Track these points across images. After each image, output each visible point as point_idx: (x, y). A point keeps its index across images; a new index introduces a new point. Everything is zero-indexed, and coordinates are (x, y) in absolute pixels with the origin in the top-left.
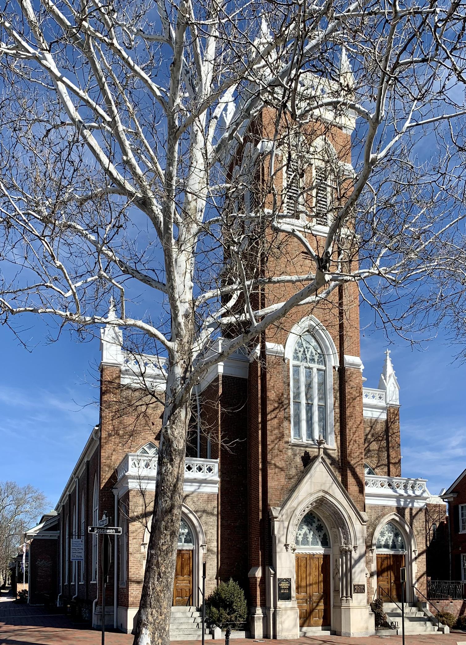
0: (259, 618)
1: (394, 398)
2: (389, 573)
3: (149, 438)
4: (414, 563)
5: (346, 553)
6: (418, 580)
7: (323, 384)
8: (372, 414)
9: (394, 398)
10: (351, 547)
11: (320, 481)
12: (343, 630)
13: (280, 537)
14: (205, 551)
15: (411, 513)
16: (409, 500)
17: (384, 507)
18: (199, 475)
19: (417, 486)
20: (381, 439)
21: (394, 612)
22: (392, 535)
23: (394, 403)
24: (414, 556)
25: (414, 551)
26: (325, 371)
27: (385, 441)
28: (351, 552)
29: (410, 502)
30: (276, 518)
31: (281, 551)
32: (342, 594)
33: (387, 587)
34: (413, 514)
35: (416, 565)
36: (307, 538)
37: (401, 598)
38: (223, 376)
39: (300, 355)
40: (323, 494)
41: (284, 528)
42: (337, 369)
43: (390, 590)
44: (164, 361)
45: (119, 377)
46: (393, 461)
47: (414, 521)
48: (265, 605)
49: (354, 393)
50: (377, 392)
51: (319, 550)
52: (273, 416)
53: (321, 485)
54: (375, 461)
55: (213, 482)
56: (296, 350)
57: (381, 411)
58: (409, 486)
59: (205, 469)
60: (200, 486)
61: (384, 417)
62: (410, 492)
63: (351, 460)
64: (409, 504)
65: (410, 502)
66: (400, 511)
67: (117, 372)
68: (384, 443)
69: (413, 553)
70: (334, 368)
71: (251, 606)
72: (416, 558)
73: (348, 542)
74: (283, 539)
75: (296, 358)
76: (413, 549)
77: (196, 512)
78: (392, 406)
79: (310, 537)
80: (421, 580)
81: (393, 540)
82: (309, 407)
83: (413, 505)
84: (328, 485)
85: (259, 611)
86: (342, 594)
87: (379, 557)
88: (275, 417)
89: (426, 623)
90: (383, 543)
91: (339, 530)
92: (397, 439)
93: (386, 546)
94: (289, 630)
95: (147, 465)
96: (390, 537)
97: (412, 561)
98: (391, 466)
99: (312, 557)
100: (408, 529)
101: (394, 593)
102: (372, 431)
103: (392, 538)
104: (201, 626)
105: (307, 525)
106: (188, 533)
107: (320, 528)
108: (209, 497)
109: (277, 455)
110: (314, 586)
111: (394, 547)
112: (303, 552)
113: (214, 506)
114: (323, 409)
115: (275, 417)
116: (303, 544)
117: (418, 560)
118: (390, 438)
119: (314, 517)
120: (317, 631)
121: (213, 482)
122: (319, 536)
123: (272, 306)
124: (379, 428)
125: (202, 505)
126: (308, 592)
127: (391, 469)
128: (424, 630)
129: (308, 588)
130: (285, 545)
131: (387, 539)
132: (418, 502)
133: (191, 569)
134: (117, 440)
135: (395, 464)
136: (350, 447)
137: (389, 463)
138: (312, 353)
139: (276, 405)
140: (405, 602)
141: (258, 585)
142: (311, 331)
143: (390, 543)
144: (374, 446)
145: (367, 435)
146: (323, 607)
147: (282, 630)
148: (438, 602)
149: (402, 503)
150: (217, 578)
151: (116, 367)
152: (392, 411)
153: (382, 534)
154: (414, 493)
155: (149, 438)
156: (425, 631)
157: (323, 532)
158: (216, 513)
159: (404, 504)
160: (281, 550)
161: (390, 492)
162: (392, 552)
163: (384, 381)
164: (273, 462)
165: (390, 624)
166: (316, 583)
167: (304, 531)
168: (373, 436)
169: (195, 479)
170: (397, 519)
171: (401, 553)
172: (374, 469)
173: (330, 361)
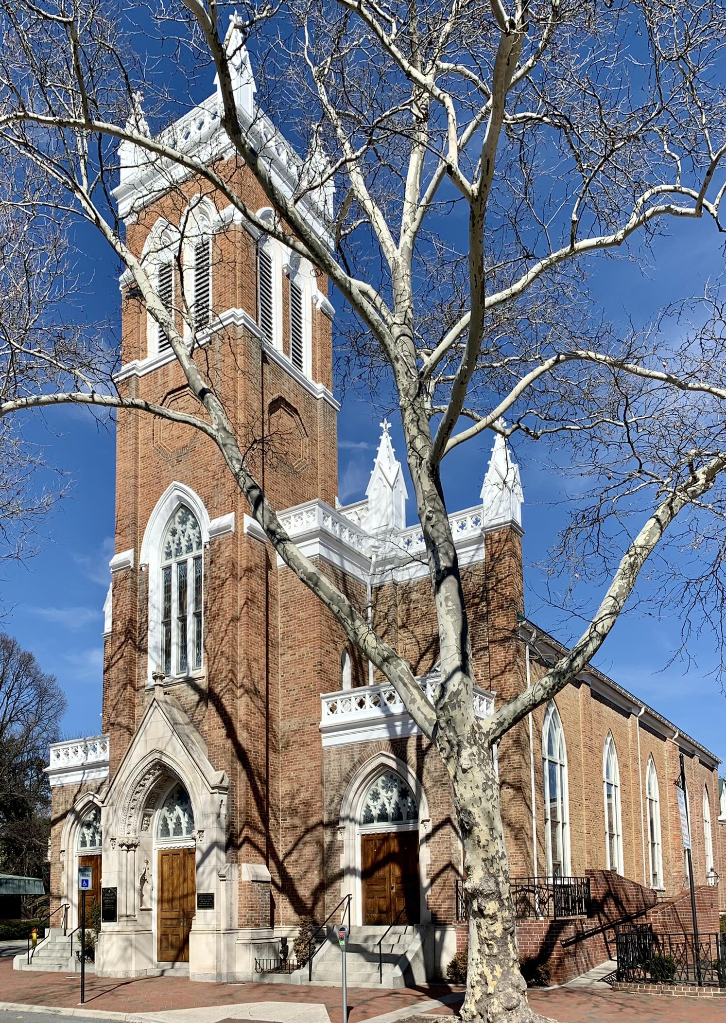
6: (433, 881)
17: (365, 744)
20: (477, 600)
22: (394, 794)
34: (424, 746)
35: (428, 850)
40: (157, 756)
47: (427, 760)
57: (475, 547)
64: (412, 728)
66: (398, 746)
72: (428, 837)
80: (439, 881)
81: (397, 804)
87: (367, 840)
90: (375, 812)
93: (383, 817)
94: (114, 965)
95: (361, 704)
111: (397, 817)
116: (175, 834)
117: (432, 840)
143: (390, 810)
149: (399, 730)
152: (496, 536)
170: (393, 764)
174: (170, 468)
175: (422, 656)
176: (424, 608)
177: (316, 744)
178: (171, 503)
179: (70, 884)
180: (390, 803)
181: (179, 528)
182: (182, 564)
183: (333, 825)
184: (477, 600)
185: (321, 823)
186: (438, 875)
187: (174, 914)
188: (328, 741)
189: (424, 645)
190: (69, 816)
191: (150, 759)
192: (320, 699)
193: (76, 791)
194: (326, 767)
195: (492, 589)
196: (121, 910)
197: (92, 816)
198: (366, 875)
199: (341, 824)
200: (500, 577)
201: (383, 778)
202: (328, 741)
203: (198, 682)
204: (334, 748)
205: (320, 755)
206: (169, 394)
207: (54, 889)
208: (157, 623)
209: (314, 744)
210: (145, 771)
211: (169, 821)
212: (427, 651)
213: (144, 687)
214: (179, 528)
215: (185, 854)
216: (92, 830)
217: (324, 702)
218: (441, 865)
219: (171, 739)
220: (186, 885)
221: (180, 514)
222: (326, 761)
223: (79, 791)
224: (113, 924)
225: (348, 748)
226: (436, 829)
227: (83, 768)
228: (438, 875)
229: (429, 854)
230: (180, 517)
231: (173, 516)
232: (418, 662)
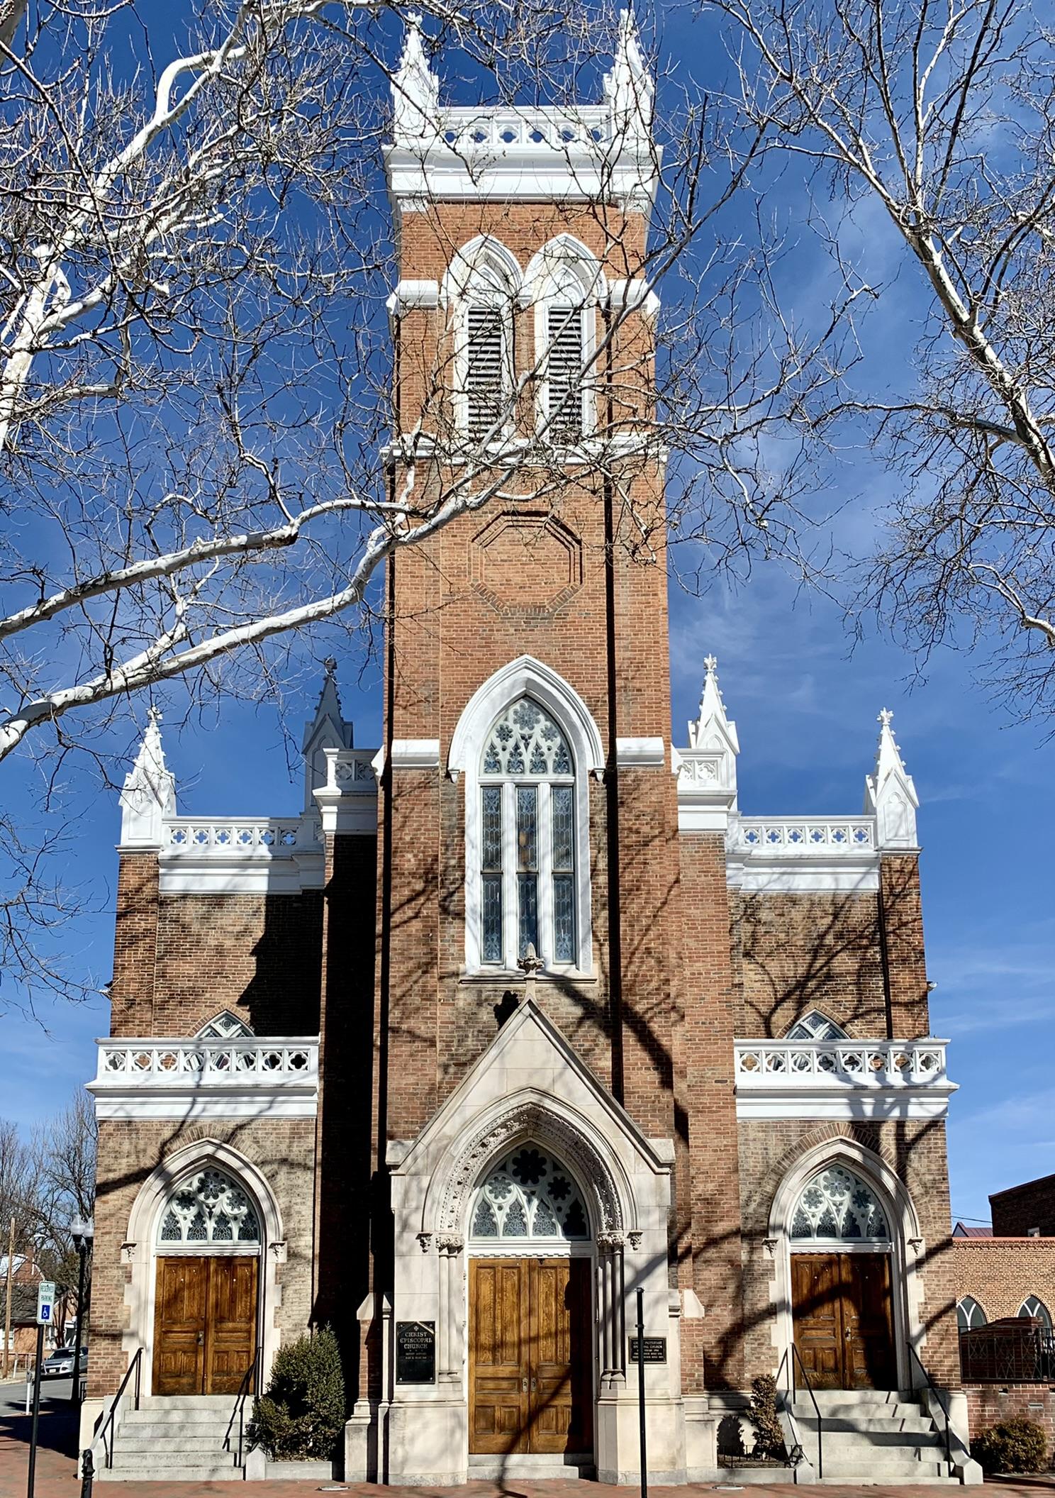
0: (357, 1428)
1: (902, 832)
2: (837, 1305)
3: (223, 1002)
4: (912, 1279)
5: (612, 1251)
6: (928, 1326)
7: (565, 821)
8: (836, 880)
9: (902, 832)
10: (622, 1236)
11: (528, 1064)
12: (602, 1467)
13: (409, 1215)
14: (282, 1258)
15: (900, 1136)
16: (890, 1100)
17: (809, 1123)
18: (272, 1077)
19: (917, 1062)
20: (865, 942)
21: (841, 1416)
22: (846, 1199)
23: (904, 845)
24: (911, 1256)
25: (911, 1242)
26: (573, 786)
27: (877, 949)
28: (622, 1248)
29: (893, 1105)
30: (396, 1167)
31: (410, 1252)
32: (605, 1367)
33: (831, 1345)
36: (523, 1215)
37: (882, 1378)
38: (338, 838)
39: (504, 757)
40: (534, 1098)
41: (420, 1191)
42: (600, 776)
43: (842, 1356)
44: (266, 825)
45: (157, 876)
46: (903, 998)
48: (375, 1396)
49: (646, 829)
50: (850, 824)
51: (558, 1246)
52: (410, 913)
53: (530, 1076)
54: (849, 1000)
55: (309, 1091)
56: (493, 747)
57: (863, 870)
58: (893, 1062)
59: (286, 1060)
60: (272, 1102)
61: (872, 884)
62: (895, 1079)
63: (637, 1003)
64: (890, 1110)
65: (893, 1105)
66: (865, 1132)
67: (152, 865)
68: (874, 954)
69: (909, 1248)
70: (593, 774)
71: (351, 1396)
72: (919, 1263)
73: (614, 1221)
74: (415, 1221)
75: (493, 764)
76: (909, 1233)
77: (263, 1163)
78: (897, 852)
79: (531, 1213)
80: (938, 1327)
81: (850, 1214)
82: (528, 884)
83: (904, 1112)
84: (549, 1075)
85: (362, 1409)
86: (605, 1367)
87: (798, 1262)
88: (416, 916)
89: (918, 1452)
90: (815, 1223)
91: (593, 1190)
92: (915, 940)
93: (827, 1229)
94: (426, 1461)
96: (838, 1206)
97: (906, 1271)
98: (895, 1011)
99: (539, 1265)
100: (890, 1183)
101: (858, 1364)
102: (838, 926)
103: (844, 1209)
104: (234, 1444)
105: (523, 1182)
106: (250, 1216)
107: (560, 1189)
108: (297, 1129)
109: (418, 1009)
110: (542, 1343)
111: (852, 1231)
112: (508, 1252)
113: (309, 1145)
114: (565, 882)
115: (416, 916)
116: (508, 1230)
117: (926, 1268)
118: (891, 939)
119: (544, 1161)
120: (544, 1467)
121: (309, 1091)
122: (559, 1209)
123: (205, 644)
124: (860, 914)
125: (275, 1147)
126: (525, 1357)
127: (896, 1021)
128: (905, 1470)
129: (524, 1349)
130: (419, 1236)
131: (828, 1212)
132: (921, 1104)
133: (254, 1302)
134: (148, 1016)
135: (908, 1005)
136: (632, 967)
137: (889, 1003)
138: (538, 747)
139: (419, 886)
140: (895, 1389)
141: (363, 1341)
142: (531, 699)
143: (840, 1221)
144: (845, 963)
145: (822, 937)
146: (569, 1401)
147: (404, 1462)
148: (1005, 1391)
149: (868, 1110)
150: (310, 1325)
151: (149, 853)
152: (897, 864)
153: (813, 1198)
154: (907, 1078)
155: (223, 1002)
156: (907, 1475)
157: (569, 1199)
158: (312, 1164)
159: (874, 1110)
160: (411, 1248)
161: (828, 1080)
162: (846, 1248)
163: (872, 791)
164: (404, 1027)
165: (789, 1450)
166: (548, 1335)
167: (511, 1198)
168: (840, 936)
169: (257, 1086)
171: (877, 1248)
172: (843, 1025)
173: (582, 759)
174: (512, 631)
175: (779, 1003)
176: (782, 936)
177: (728, 1111)
178: (513, 686)
179: (141, 1307)
180: (838, 1210)
181: (517, 730)
182: (527, 792)
183: (757, 1234)
184: (865, 942)
185: (737, 1233)
186: (937, 1318)
187: (506, 1370)
188: (745, 1110)
189: (781, 988)
190: (151, 1178)
191: (514, 1102)
192: (732, 1045)
193: (167, 1133)
194: (741, 1148)
195: (893, 932)
196: (441, 1363)
197: (196, 1184)
198: (801, 1311)
199: (771, 1237)
200: (905, 919)
201: (826, 1173)
202: (745, 1110)
203: (580, 986)
204: (754, 1122)
205: (731, 1129)
206: (504, 514)
207: (99, 1315)
208: (474, 872)
209: (723, 1112)
210: (499, 1122)
211: (495, 1209)
212: (787, 996)
213: (456, 974)
214: (517, 730)
215: (531, 1269)
216: (194, 1210)
217: (736, 1050)
218: (942, 1304)
219: (561, 1074)
220: (534, 1320)
221: (517, 706)
222: (741, 1139)
223: (176, 1135)
224: (424, 1387)
225: (779, 1125)
226: (931, 1253)
227: (197, 1092)
228: (937, 1318)
229: (922, 1288)
230: (516, 712)
231: (506, 708)
232: (774, 1010)
